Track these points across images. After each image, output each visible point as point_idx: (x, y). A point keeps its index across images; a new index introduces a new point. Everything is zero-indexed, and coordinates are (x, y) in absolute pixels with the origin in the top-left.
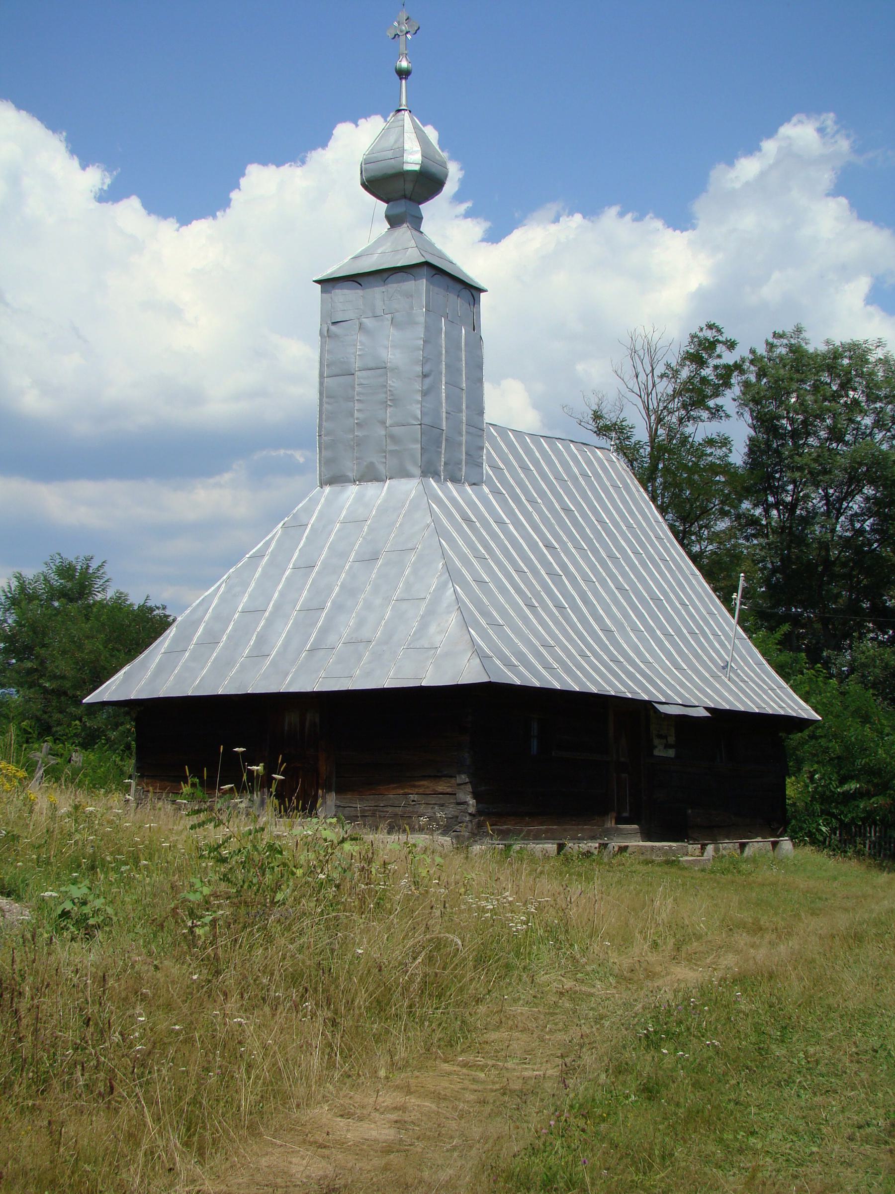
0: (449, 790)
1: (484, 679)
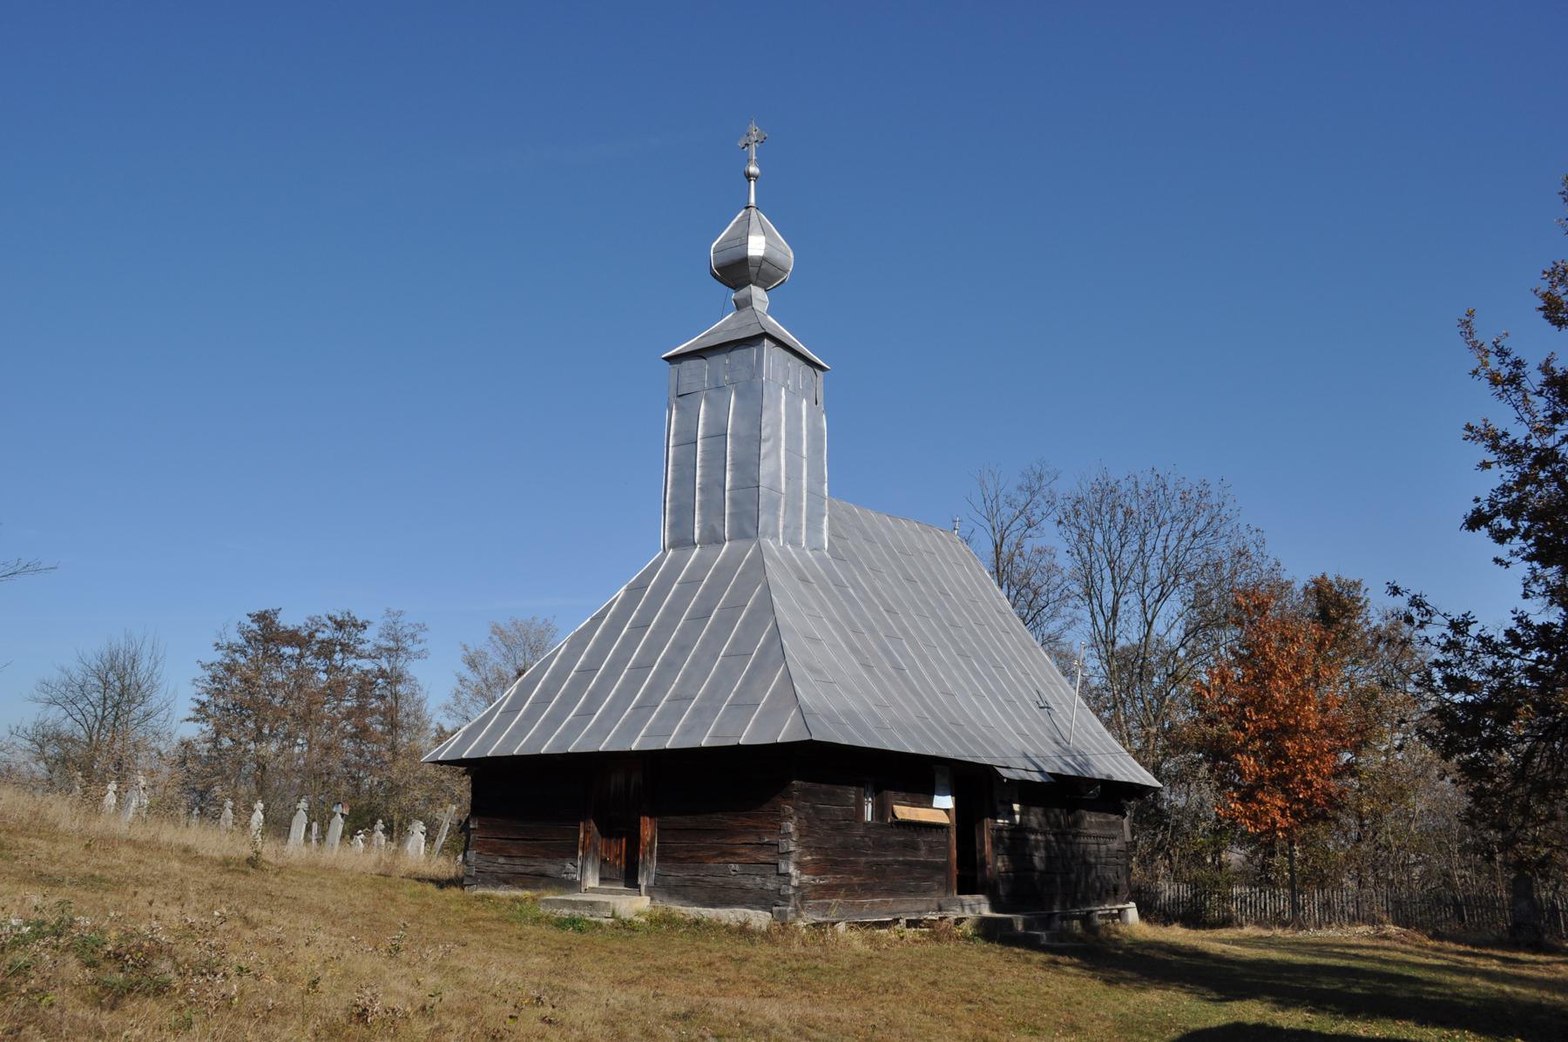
0: (770, 860)
1: (807, 737)
